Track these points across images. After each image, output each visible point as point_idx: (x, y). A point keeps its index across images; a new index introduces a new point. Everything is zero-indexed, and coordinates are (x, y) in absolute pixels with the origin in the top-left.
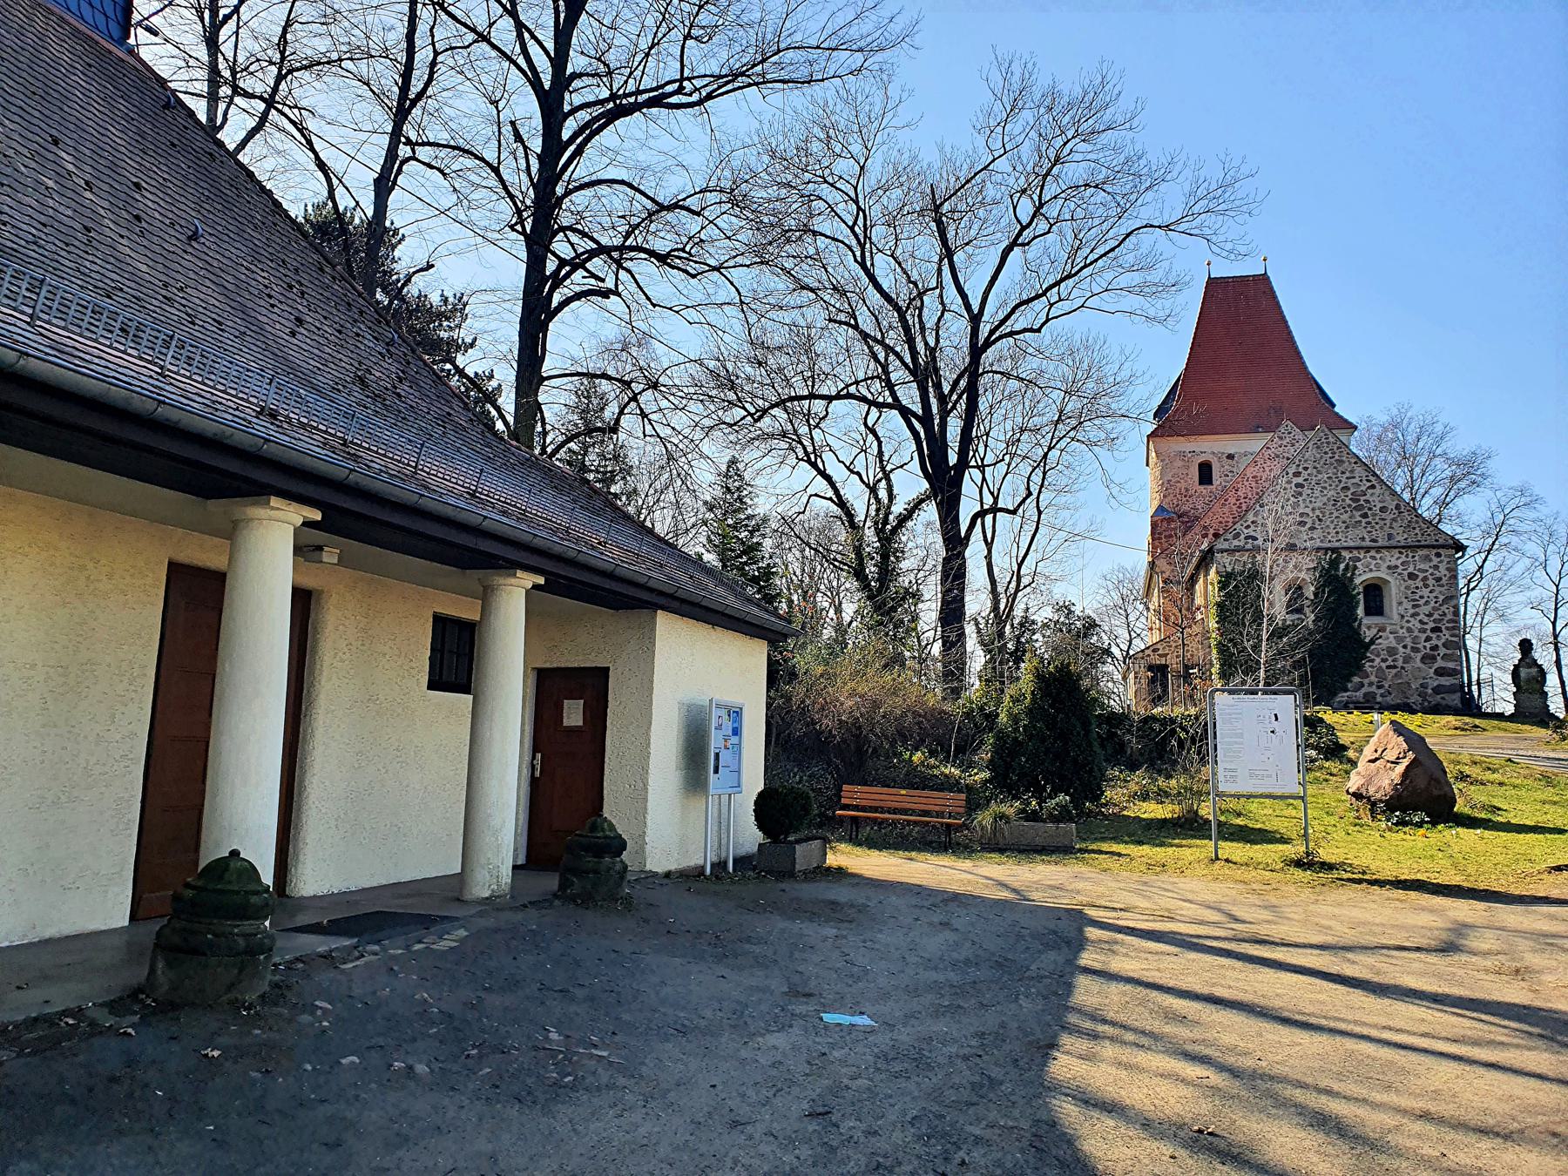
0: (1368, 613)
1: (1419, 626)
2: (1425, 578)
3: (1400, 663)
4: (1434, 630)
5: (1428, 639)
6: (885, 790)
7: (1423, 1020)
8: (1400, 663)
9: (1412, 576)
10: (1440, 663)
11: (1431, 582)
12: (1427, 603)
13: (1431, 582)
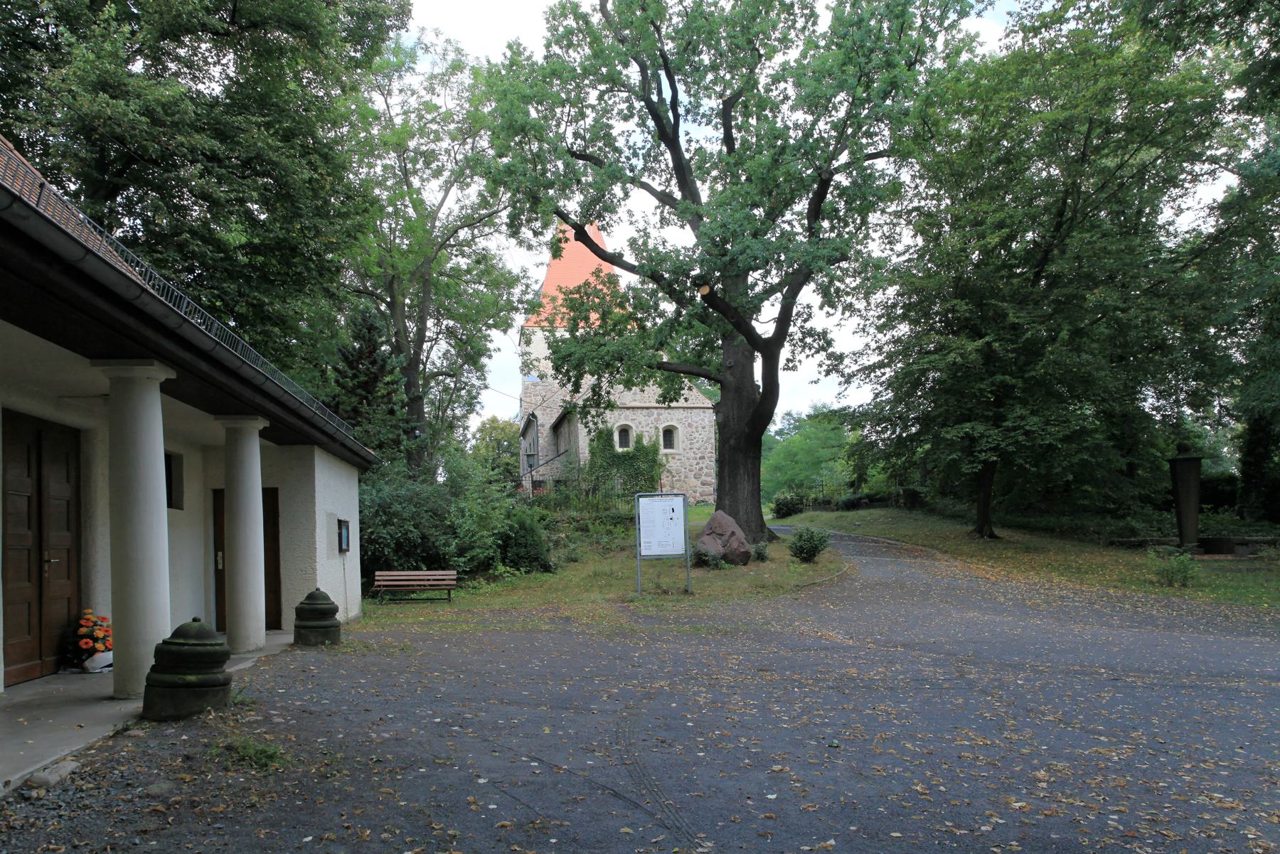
0: (666, 447)
1: (693, 455)
2: (697, 428)
3: (682, 478)
4: (700, 458)
5: (698, 464)
6: (387, 573)
7: (596, 574)
8: (682, 478)
9: (690, 425)
10: (704, 478)
11: (700, 429)
12: (698, 442)
13: (700, 429)
